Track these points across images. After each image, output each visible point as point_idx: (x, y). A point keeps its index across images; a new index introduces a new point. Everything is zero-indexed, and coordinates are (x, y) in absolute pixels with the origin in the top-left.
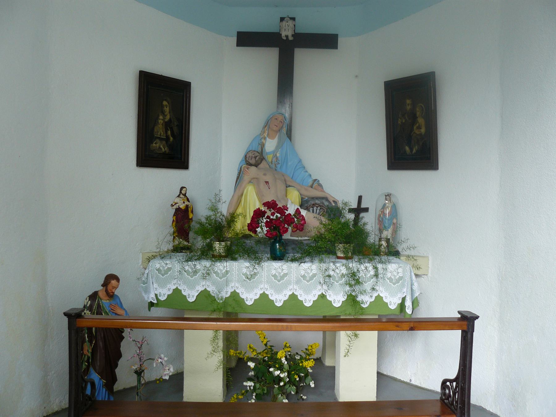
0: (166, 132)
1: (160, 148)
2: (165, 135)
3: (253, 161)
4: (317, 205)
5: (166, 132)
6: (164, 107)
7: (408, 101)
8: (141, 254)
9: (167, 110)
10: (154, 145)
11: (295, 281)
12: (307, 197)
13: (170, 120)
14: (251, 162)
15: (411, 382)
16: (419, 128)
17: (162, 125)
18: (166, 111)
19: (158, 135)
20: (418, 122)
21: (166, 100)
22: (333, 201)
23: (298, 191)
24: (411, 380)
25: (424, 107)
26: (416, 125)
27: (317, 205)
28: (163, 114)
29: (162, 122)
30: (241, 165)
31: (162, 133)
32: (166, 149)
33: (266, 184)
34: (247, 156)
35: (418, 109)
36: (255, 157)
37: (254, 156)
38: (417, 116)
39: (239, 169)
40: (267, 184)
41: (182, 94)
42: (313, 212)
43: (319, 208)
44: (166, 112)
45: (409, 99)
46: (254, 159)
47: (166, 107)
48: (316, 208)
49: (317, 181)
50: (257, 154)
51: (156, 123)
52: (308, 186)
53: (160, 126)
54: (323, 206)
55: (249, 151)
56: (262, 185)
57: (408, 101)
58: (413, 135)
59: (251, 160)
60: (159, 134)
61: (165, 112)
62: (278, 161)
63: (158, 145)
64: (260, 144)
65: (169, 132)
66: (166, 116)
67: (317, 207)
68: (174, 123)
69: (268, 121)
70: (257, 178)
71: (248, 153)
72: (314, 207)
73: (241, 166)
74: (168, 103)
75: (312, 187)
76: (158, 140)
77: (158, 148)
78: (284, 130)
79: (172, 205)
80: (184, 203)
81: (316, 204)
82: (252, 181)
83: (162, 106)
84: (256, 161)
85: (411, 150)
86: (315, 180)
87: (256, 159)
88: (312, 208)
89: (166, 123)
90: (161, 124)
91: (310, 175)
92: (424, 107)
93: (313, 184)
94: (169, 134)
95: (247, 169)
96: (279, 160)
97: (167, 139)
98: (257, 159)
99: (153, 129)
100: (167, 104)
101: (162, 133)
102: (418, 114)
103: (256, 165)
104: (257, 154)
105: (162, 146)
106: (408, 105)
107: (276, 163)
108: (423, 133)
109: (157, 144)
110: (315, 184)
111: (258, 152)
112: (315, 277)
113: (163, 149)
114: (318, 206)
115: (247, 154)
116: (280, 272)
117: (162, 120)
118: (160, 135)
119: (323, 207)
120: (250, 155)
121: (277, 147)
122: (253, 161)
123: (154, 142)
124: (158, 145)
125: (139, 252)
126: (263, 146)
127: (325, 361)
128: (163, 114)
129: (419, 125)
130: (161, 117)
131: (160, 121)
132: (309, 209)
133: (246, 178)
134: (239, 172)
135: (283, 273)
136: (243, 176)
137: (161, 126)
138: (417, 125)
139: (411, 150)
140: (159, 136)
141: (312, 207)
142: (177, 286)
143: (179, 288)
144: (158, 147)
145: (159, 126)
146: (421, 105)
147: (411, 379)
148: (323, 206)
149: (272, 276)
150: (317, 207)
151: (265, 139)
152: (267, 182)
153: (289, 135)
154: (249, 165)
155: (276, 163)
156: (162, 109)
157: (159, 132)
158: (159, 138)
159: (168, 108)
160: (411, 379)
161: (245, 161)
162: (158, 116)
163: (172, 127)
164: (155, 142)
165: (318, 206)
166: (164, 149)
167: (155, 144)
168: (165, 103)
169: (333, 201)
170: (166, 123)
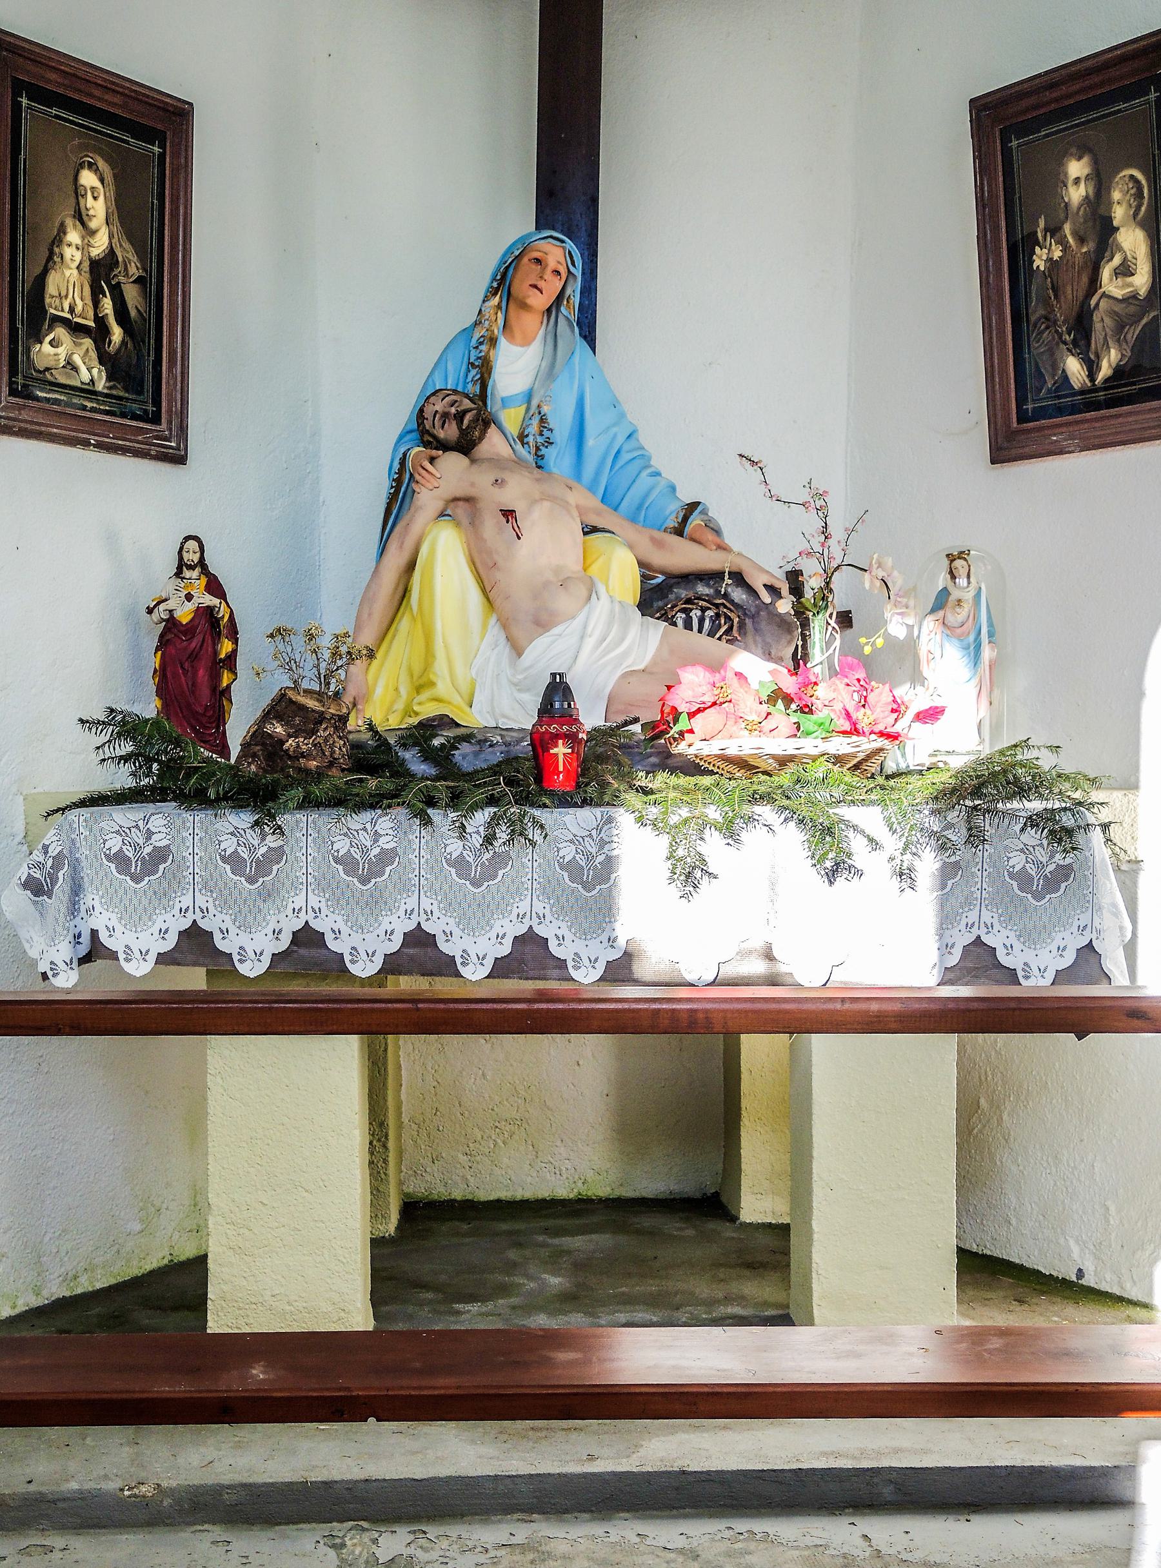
0: (96, 304)
1: (70, 365)
2: (91, 314)
3: (450, 432)
4: (701, 603)
5: (96, 304)
6: (84, 196)
7: (1076, 168)
8: (22, 798)
9: (97, 208)
10: (46, 348)
11: (539, 883)
12: (663, 573)
13: (111, 252)
14: (441, 434)
15: (1083, 1282)
16: (1125, 270)
17: (78, 268)
18: (91, 212)
19: (63, 310)
20: (1120, 249)
21: (91, 166)
22: (765, 585)
23: (631, 547)
24: (1080, 1273)
25: (1144, 182)
26: (1112, 259)
27: (704, 600)
28: (83, 224)
29: (78, 256)
30: (402, 450)
31: (79, 302)
32: (95, 371)
33: (504, 520)
34: (429, 412)
35: (1116, 195)
36: (460, 416)
37: (453, 410)
38: (1115, 223)
39: (396, 466)
40: (508, 522)
41: (156, 149)
42: (688, 626)
43: (709, 613)
44: (94, 219)
45: (1079, 159)
46: (454, 424)
47: (95, 198)
48: (699, 613)
49: (700, 508)
50: (467, 404)
51: (51, 259)
52: (665, 531)
53: (71, 273)
54: (725, 607)
55: (433, 394)
56: (491, 524)
57: (1076, 168)
58: (1097, 305)
59: (443, 427)
60: (66, 308)
61: (90, 217)
62: (546, 433)
63: (62, 351)
64: (472, 364)
65: (107, 305)
66: (93, 233)
67: (703, 610)
68: (126, 269)
69: (507, 268)
70: (468, 500)
71: (428, 398)
72: (691, 610)
73: (405, 455)
74: (102, 180)
75: (679, 531)
76: (60, 332)
77: (62, 363)
78: (569, 312)
79: (148, 608)
80: (189, 597)
81: (699, 598)
82: (449, 512)
83: (78, 192)
84: (463, 433)
85: (1092, 367)
86: (693, 506)
87: (462, 423)
88: (684, 616)
89: (95, 265)
90: (77, 263)
91: (673, 488)
92: (1144, 182)
93: (685, 519)
94: (107, 311)
95: (431, 463)
96: (551, 430)
97: (100, 333)
98: (466, 422)
99: (40, 283)
100: (97, 184)
101: (79, 302)
102: (1119, 213)
103: (465, 446)
104: (467, 404)
105: (77, 360)
106: (1077, 181)
107: (540, 440)
108: (1143, 292)
109: (57, 347)
110: (695, 521)
111: (467, 396)
112: (165, 862)
113: (83, 369)
114: (704, 604)
115: (424, 405)
116: (593, 851)
117: (78, 249)
118: (72, 310)
119: (725, 610)
120: (439, 407)
121: (550, 373)
122: (450, 432)
123: (48, 339)
124: (62, 351)
125: (14, 789)
126: (484, 368)
127: (739, 1208)
128: (83, 224)
129: (1125, 259)
130: (73, 236)
131: (68, 252)
132: (673, 617)
133: (427, 500)
134: (396, 476)
135: (1054, 866)
136: (414, 491)
137: (75, 272)
138: (1117, 260)
139: (1092, 367)
140: (69, 316)
141: (683, 610)
142: (194, 917)
143: (202, 924)
144: (62, 357)
145: (67, 273)
146: (1132, 177)
147: (1080, 1270)
148: (725, 607)
149: (225, 859)
150: (703, 610)
151: (493, 341)
152: (508, 514)
153: (588, 331)
154: (437, 449)
155: (540, 440)
156: (78, 203)
157: (66, 296)
158: (66, 322)
159: (101, 199)
160: (1080, 1270)
161: (415, 435)
162: (62, 230)
163: (119, 283)
164: (51, 336)
165: (704, 604)
166: (89, 370)
167: (51, 343)
168: (88, 178)
169: (765, 585)
170: (95, 265)
